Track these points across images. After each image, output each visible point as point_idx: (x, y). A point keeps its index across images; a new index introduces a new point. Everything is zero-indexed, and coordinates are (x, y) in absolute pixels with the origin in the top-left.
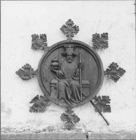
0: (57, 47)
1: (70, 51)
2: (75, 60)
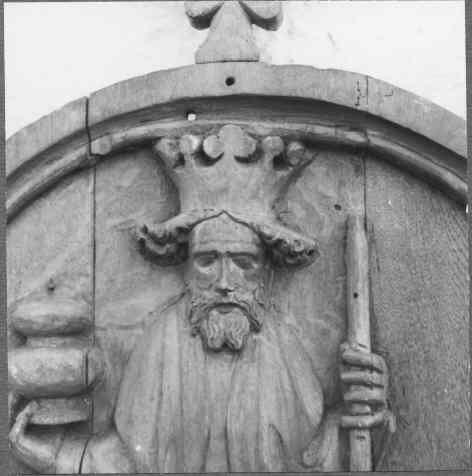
0: (72, 157)
1: (231, 205)
2: (290, 319)
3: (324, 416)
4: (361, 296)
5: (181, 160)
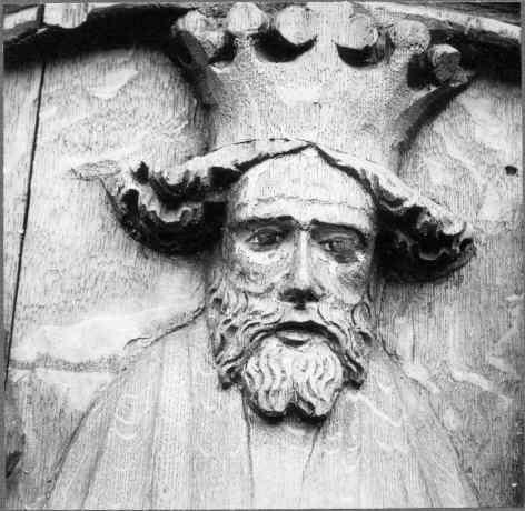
5: (228, 51)
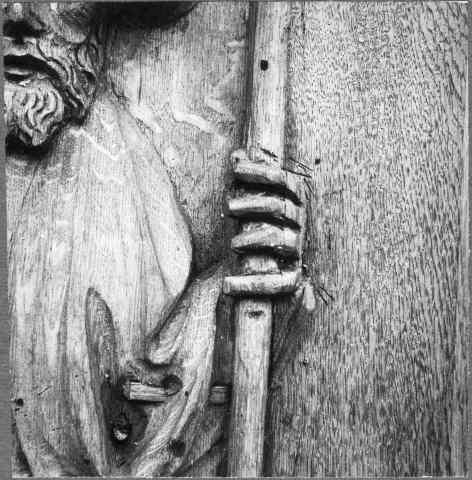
3: (191, 281)
4: (273, 67)
